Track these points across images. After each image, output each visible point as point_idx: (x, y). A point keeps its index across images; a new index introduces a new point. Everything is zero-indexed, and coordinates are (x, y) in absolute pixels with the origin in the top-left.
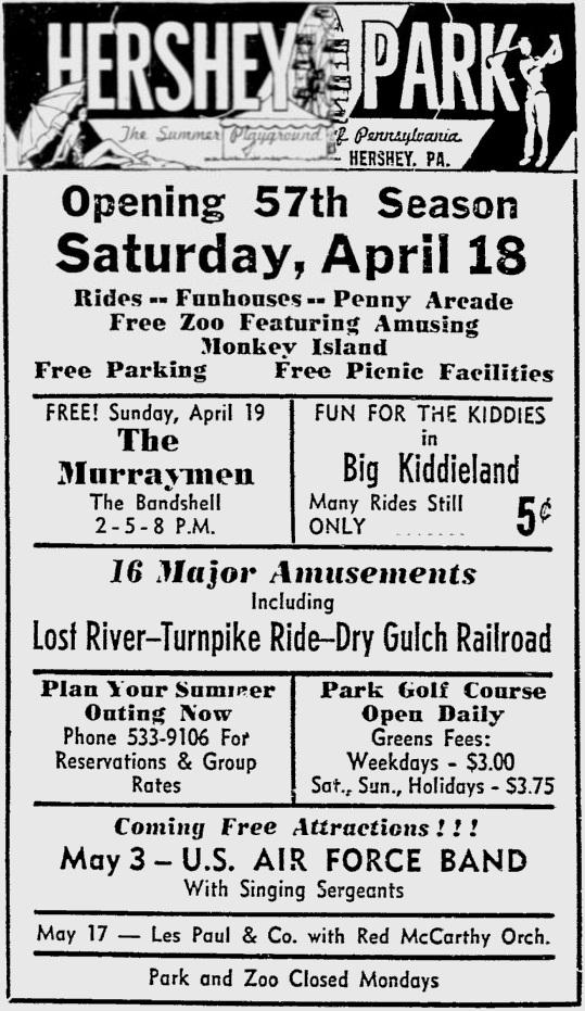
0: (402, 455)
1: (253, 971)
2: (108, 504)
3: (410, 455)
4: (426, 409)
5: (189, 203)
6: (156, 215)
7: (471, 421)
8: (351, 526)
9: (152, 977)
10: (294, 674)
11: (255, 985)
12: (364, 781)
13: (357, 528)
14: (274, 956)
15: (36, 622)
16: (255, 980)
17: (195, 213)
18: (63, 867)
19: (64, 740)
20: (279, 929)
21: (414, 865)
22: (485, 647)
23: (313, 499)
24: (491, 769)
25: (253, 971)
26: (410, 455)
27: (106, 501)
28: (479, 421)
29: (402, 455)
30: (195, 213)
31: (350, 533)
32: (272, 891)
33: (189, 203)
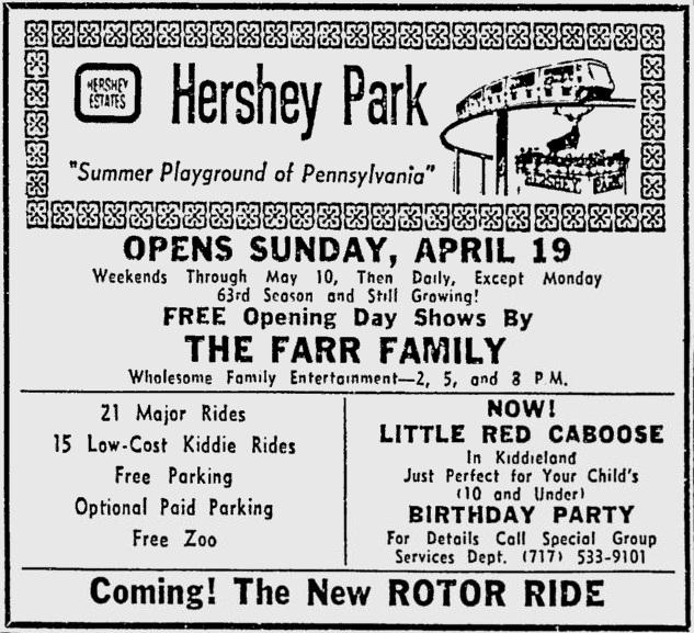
0: (185, 437)
1: (193, 532)
2: (265, 593)
3: (192, 437)
4: (414, 431)
5: (175, 593)
6: (459, 338)
7: (185, 451)
8: (480, 350)
9: (171, 476)
10: (461, 151)
11: (194, 545)
12: (260, 244)
13: (490, 353)
14: (292, 392)
15: (90, 437)
16: (195, 540)
17: (180, 601)
18: (368, 589)
19: (196, 502)
20: (139, 438)
21: (595, 599)
22: (425, 518)
23: (140, 411)
24: (125, 447)
25: (193, 532)
26: (192, 437)
27: (260, 590)
28: (193, 451)
29: (185, 437)
30: (180, 601)
31: (480, 360)
32: (207, 175)
33: (175, 593)
